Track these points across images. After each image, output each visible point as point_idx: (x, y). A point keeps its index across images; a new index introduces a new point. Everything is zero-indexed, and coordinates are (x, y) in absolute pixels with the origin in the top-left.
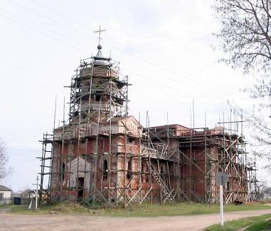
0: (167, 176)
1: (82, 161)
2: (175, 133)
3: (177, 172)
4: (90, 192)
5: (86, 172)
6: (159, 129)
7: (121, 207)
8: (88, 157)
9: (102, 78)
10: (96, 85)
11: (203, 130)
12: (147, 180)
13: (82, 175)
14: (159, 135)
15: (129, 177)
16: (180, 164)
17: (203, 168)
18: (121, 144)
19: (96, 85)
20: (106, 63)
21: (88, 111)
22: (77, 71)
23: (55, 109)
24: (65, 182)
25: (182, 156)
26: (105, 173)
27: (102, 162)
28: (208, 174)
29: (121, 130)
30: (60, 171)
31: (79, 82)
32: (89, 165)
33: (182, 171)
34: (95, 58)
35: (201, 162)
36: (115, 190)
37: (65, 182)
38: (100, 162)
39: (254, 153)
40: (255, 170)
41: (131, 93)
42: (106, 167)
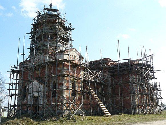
0: (102, 94)
1: (36, 83)
2: (107, 64)
3: (109, 91)
4: (43, 107)
5: (39, 92)
6: (95, 62)
7: (93, 61)
8: (41, 80)
9: (51, 23)
10: (48, 28)
11: (127, 61)
12: (88, 98)
13: (36, 94)
14: (96, 66)
15: (73, 94)
16: (111, 86)
17: (129, 88)
18: (66, 68)
19: (48, 28)
20: (55, 13)
21: (41, 46)
22: (34, 19)
23: (17, 49)
24: (26, 100)
25: (112, 80)
26: (54, 92)
27: (51, 84)
28: (132, 92)
29: (66, 57)
30: (23, 93)
31: (36, 26)
32: (42, 86)
33: (112, 91)
34: (47, 9)
35: (127, 82)
36: (62, 104)
37: (26, 100)
38: (50, 84)
39: (159, 79)
40: (160, 90)
41: (74, 35)
42: (54, 86)
